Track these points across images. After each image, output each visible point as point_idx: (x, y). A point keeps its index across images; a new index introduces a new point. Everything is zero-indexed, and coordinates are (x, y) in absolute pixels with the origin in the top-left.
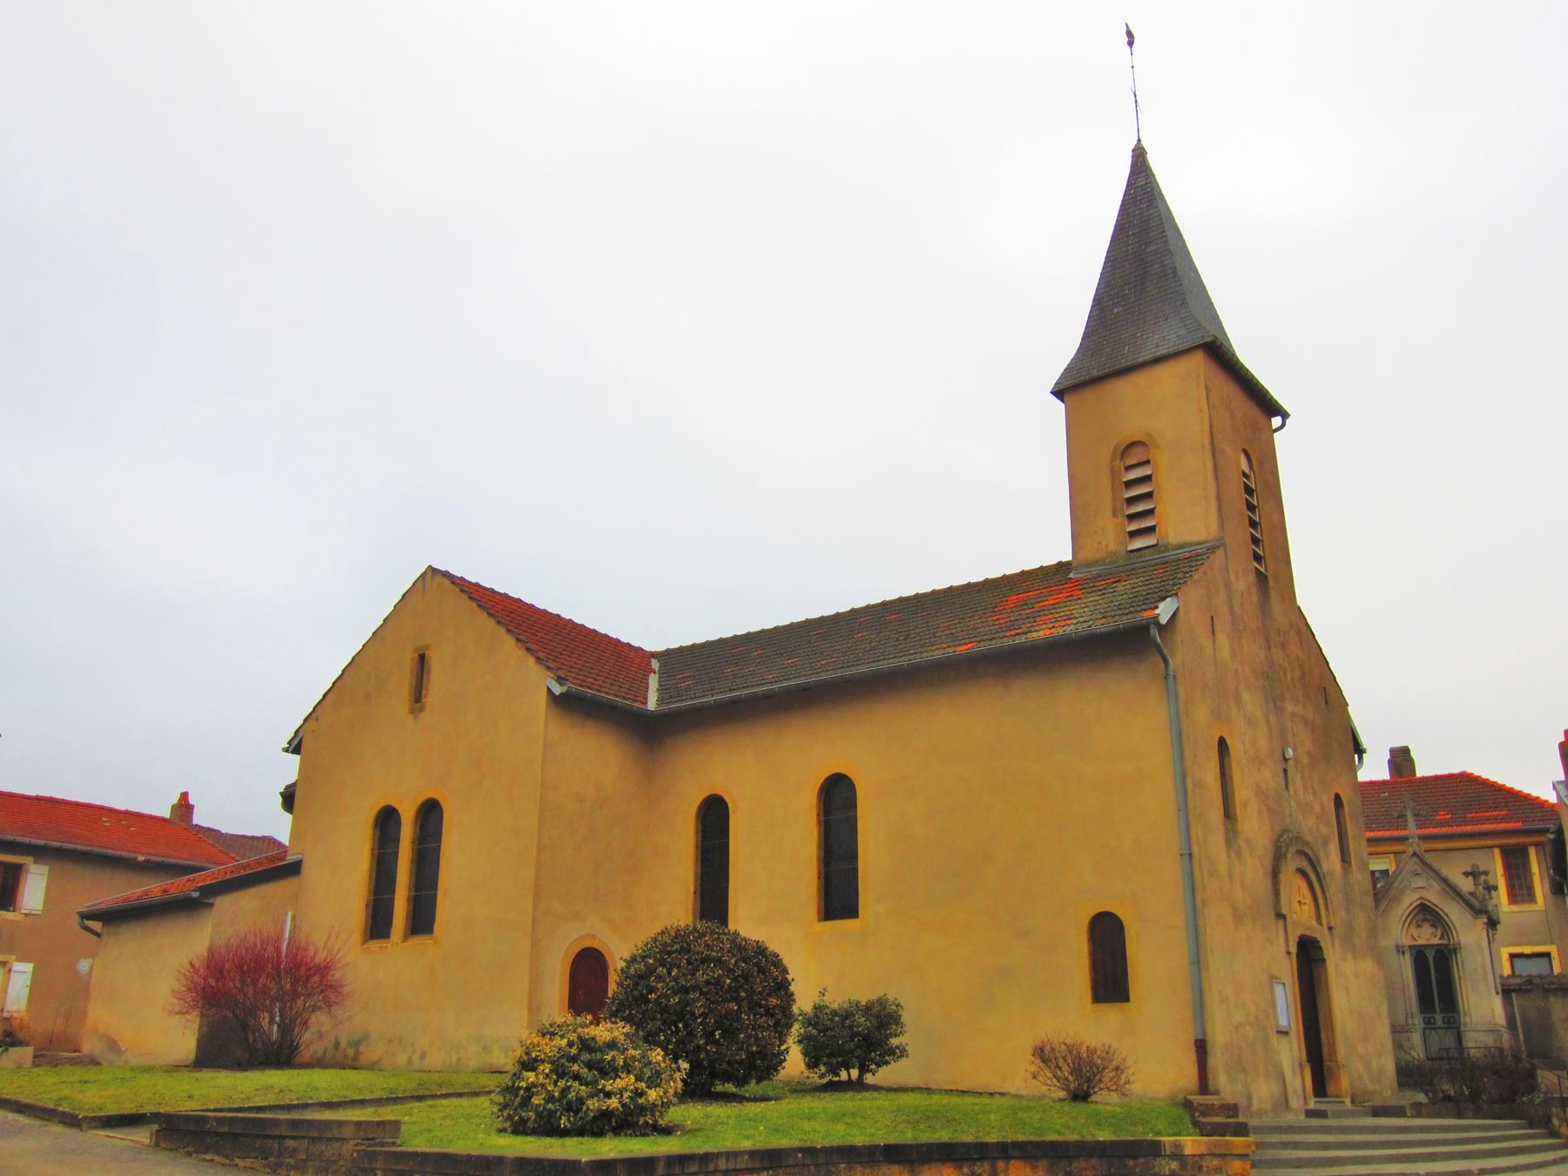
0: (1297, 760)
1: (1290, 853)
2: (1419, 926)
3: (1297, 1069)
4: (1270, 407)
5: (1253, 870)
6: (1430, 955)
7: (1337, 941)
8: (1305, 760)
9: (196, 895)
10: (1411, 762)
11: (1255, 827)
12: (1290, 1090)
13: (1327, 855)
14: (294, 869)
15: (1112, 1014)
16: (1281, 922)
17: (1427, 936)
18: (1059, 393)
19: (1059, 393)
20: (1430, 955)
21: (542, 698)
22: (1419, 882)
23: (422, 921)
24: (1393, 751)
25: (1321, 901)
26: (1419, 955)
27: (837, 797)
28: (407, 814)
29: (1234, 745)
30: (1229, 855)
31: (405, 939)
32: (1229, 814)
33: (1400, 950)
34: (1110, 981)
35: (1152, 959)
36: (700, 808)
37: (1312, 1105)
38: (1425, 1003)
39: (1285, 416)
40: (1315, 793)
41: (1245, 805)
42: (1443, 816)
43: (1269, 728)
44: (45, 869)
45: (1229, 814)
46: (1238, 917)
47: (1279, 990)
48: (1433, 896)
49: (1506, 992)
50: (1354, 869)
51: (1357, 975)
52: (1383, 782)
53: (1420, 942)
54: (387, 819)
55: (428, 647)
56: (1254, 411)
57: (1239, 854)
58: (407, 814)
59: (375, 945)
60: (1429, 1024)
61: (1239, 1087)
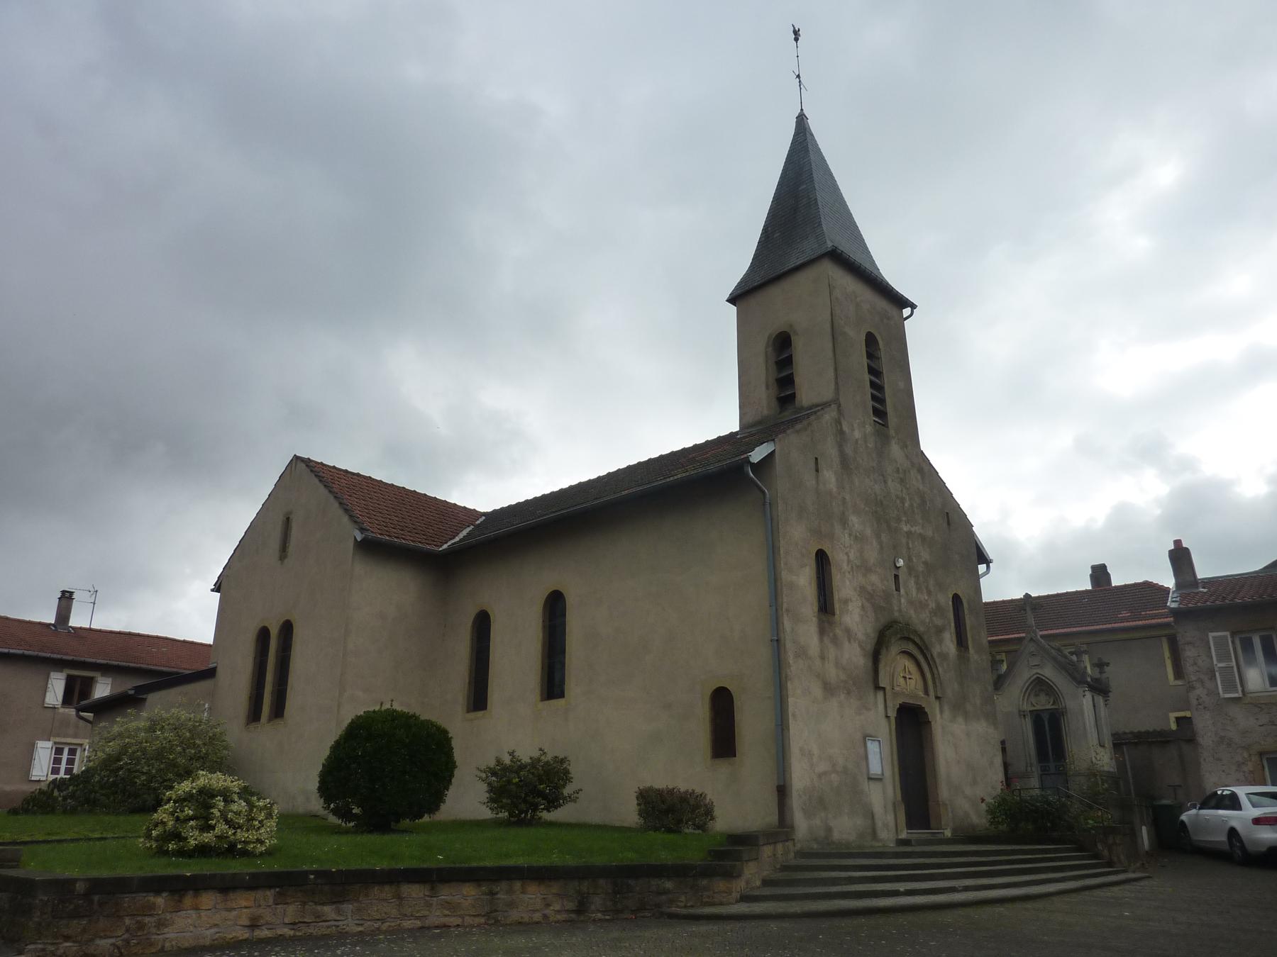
0: (910, 568)
1: (891, 635)
2: (1036, 695)
3: (890, 807)
4: (901, 302)
5: (854, 656)
6: (1046, 717)
7: (946, 708)
8: (921, 568)
9: (132, 692)
10: (1108, 576)
11: (855, 618)
12: (879, 824)
13: (941, 641)
14: (210, 673)
15: (724, 767)
16: (880, 695)
17: (1043, 703)
18: (733, 300)
19: (733, 300)
20: (1046, 717)
21: (351, 544)
22: (1036, 661)
23: (278, 711)
24: (1094, 568)
25: (928, 676)
26: (1037, 718)
27: (555, 605)
28: (274, 632)
29: (841, 558)
30: (821, 640)
31: (270, 720)
32: (826, 606)
33: (1023, 714)
34: (724, 742)
35: (751, 724)
36: (474, 622)
37: (903, 835)
38: (1042, 754)
39: (913, 306)
40: (929, 593)
41: (846, 602)
42: (1125, 614)
43: (881, 543)
44: (109, 680)
45: (826, 606)
46: (829, 689)
47: (873, 747)
48: (1048, 672)
49: (1117, 746)
50: (971, 650)
51: (968, 734)
52: (1086, 591)
53: (1038, 707)
54: (264, 634)
55: (291, 513)
56: (882, 304)
57: (835, 641)
58: (274, 632)
59: (252, 726)
60: (1045, 772)
61: (817, 822)
